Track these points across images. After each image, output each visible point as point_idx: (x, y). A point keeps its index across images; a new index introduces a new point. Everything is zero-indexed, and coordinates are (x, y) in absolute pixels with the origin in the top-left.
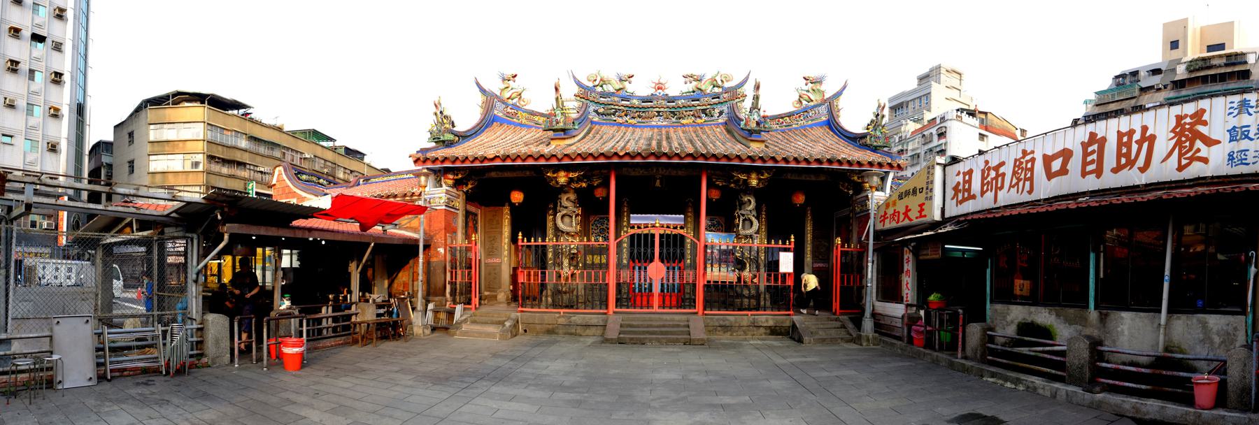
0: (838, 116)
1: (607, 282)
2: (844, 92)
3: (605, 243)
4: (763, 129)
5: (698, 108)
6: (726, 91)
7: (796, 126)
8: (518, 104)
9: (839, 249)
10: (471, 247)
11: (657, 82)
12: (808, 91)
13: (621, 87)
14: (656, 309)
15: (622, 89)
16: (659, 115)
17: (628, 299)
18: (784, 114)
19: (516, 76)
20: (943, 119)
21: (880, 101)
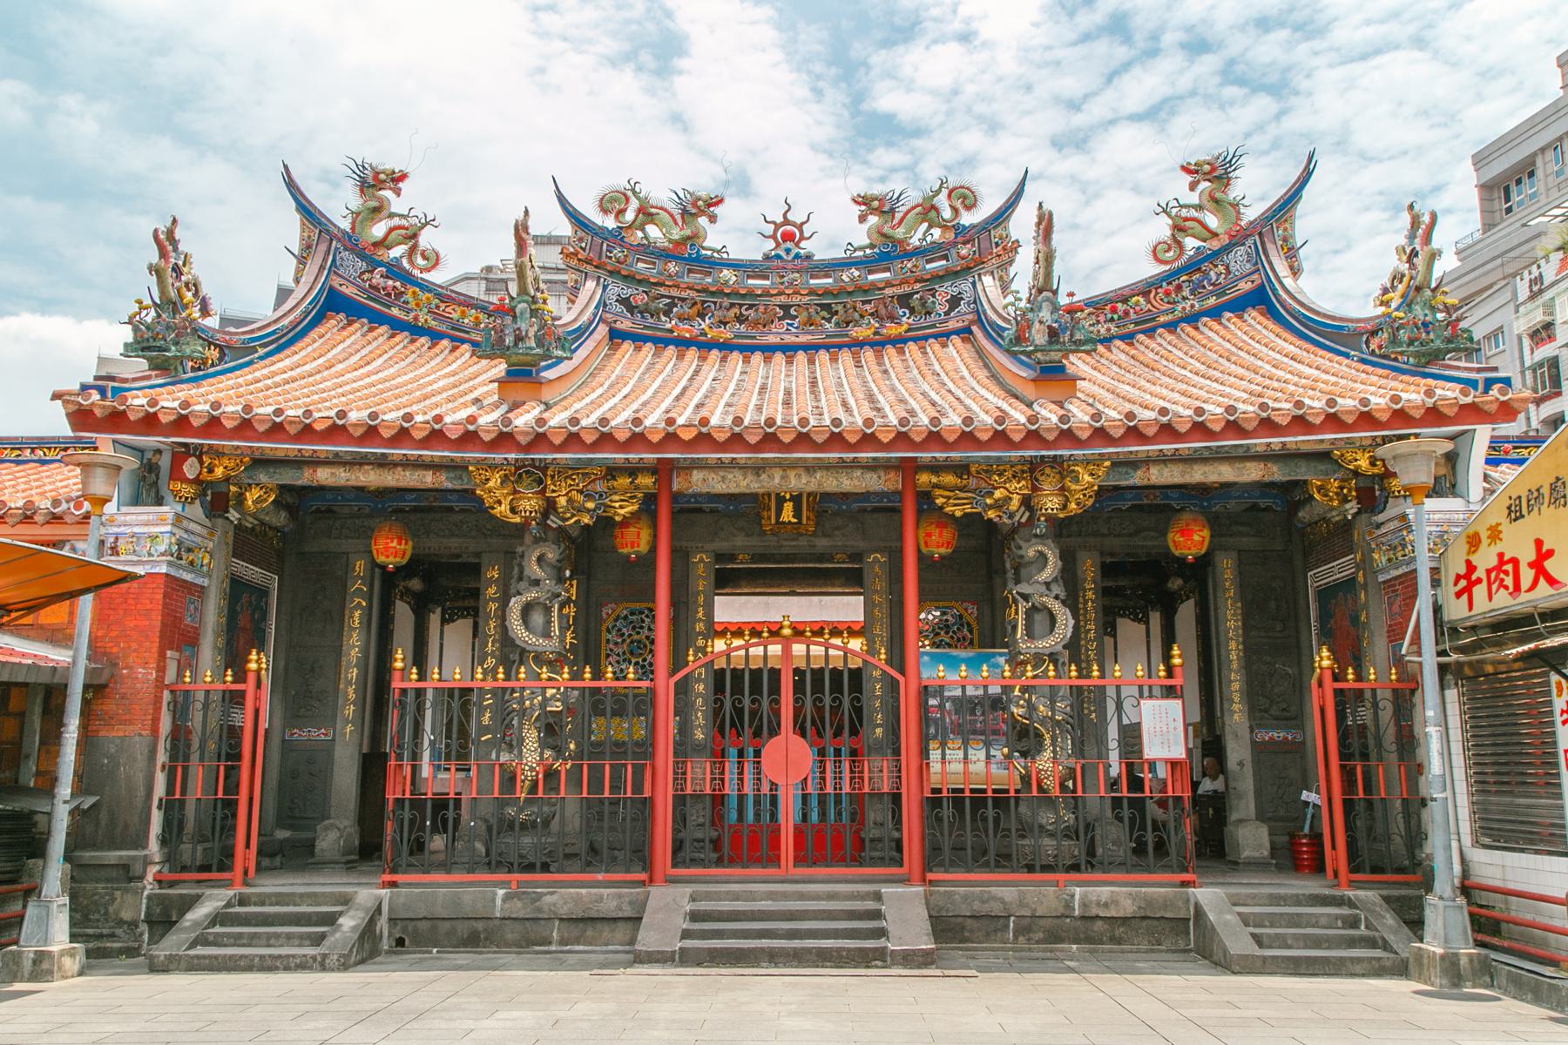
1: (647, 794)
2: (1307, 192)
3: (645, 684)
5: (889, 291)
6: (964, 235)
7: (1170, 317)
9: (1329, 685)
10: (242, 694)
11: (780, 219)
12: (1199, 208)
16: (787, 315)
17: (499, 864)
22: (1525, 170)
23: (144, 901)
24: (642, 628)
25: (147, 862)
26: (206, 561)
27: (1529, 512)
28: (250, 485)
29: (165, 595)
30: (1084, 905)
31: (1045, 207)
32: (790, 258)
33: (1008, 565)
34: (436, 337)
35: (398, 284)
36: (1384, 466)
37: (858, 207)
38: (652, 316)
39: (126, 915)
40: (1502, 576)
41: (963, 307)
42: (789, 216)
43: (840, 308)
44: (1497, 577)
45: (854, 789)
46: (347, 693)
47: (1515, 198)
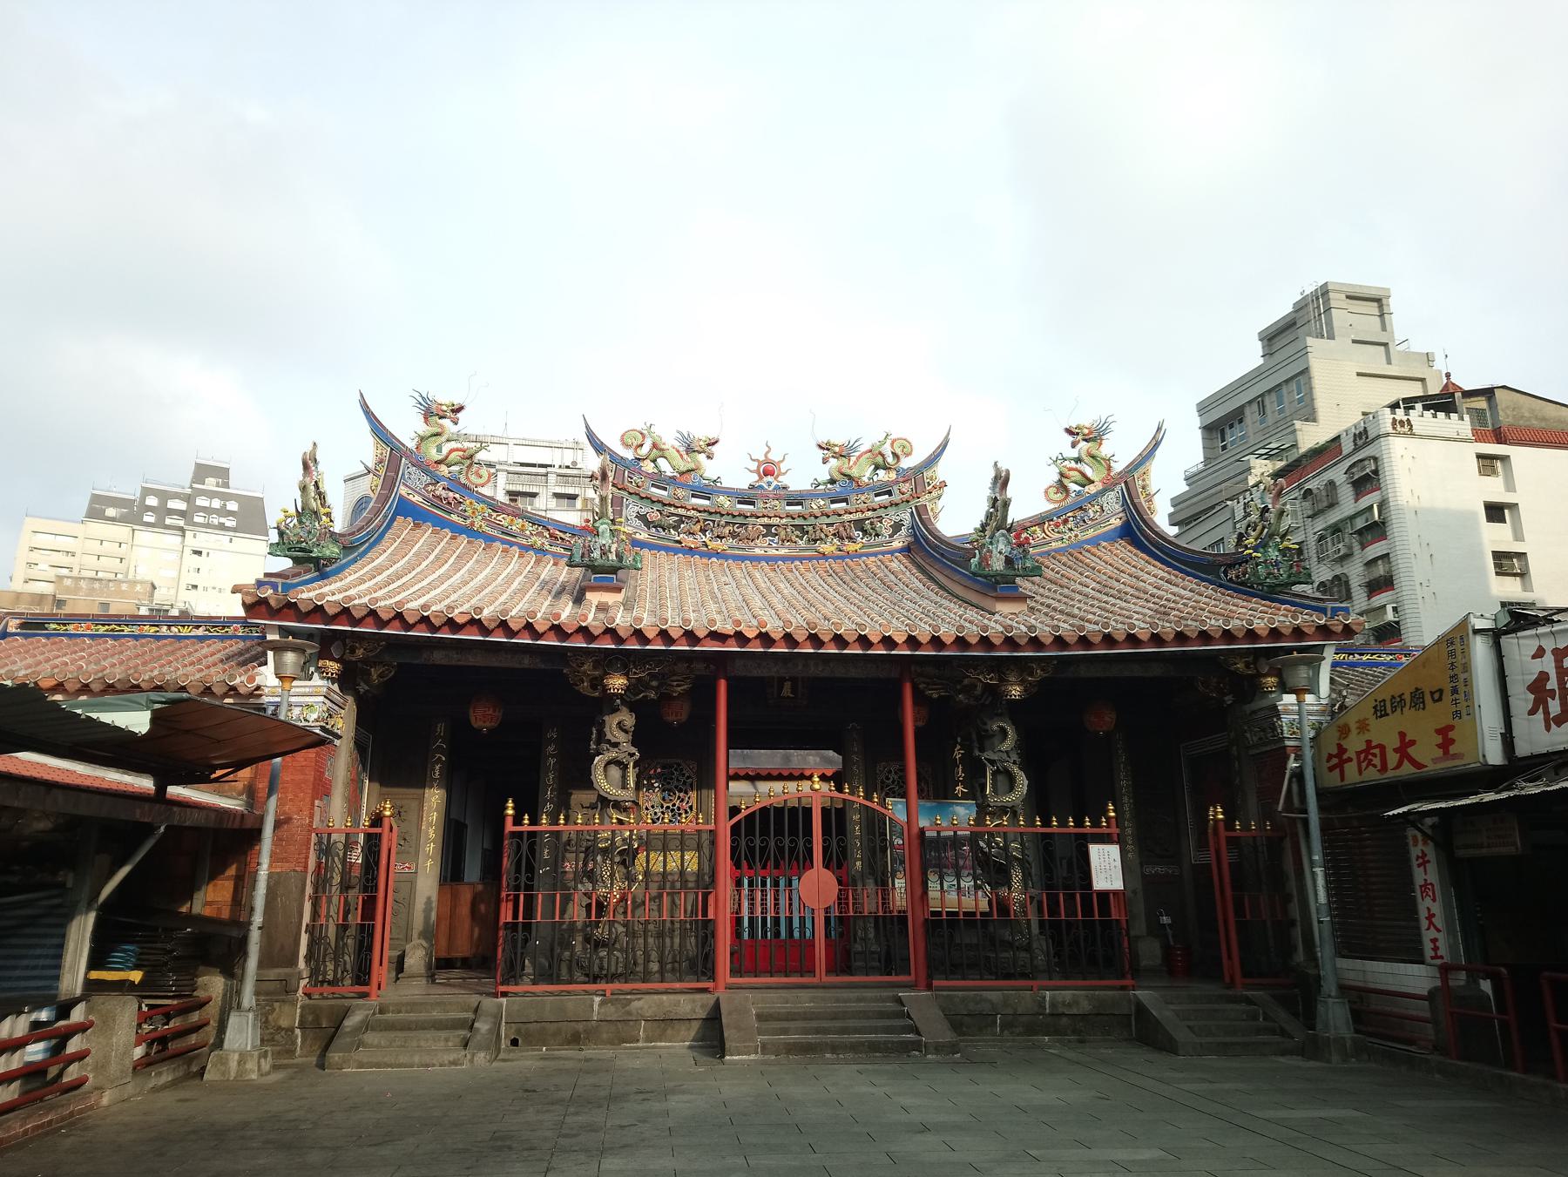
2: (1158, 452)
5: (847, 517)
8: (463, 480)
11: (762, 458)
13: (692, 466)
20: (1363, 437)
22: (1236, 417)
23: (298, 1011)
24: (672, 779)
27: (1393, 712)
30: (1053, 1005)
31: (999, 465)
32: (771, 489)
34: (490, 539)
35: (457, 496)
37: (822, 451)
38: (664, 531)
39: (284, 1023)
40: (1370, 757)
41: (904, 531)
43: (811, 528)
44: (1365, 758)
45: (841, 912)
47: (1229, 439)
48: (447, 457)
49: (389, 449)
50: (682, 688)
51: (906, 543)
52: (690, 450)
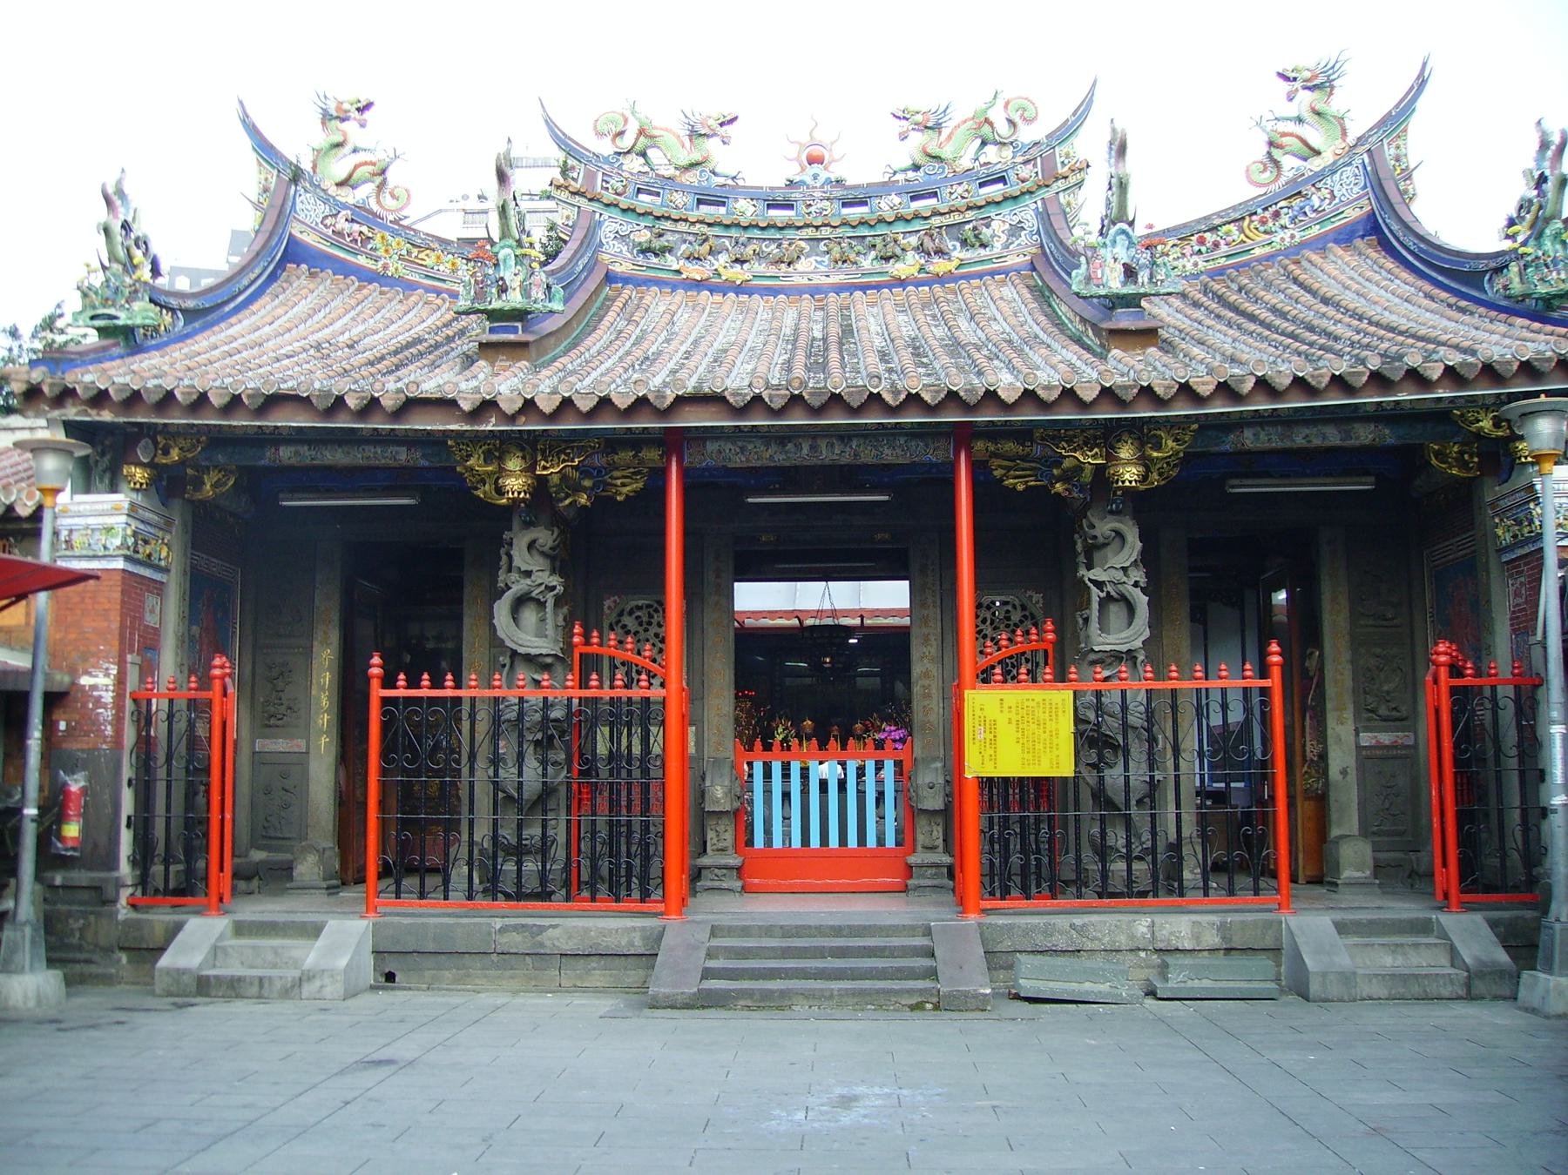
0: (1407, 198)
2: (1421, 104)
4: (1147, 289)
5: (936, 221)
7: (1267, 249)
8: (375, 207)
10: (210, 703)
11: (806, 139)
12: (1300, 120)
13: (696, 157)
14: (458, 896)
15: (698, 164)
18: (1218, 214)
19: (368, 106)
21: (1546, 125)
25: (119, 884)
26: (164, 554)
28: (208, 468)
29: (123, 592)
33: (1079, 547)
35: (364, 229)
36: (1510, 427)
41: (1024, 238)
42: (814, 134)
43: (878, 241)
46: (319, 698)
48: (350, 176)
49: (275, 172)
50: (628, 488)
51: (1028, 258)
52: (694, 134)
